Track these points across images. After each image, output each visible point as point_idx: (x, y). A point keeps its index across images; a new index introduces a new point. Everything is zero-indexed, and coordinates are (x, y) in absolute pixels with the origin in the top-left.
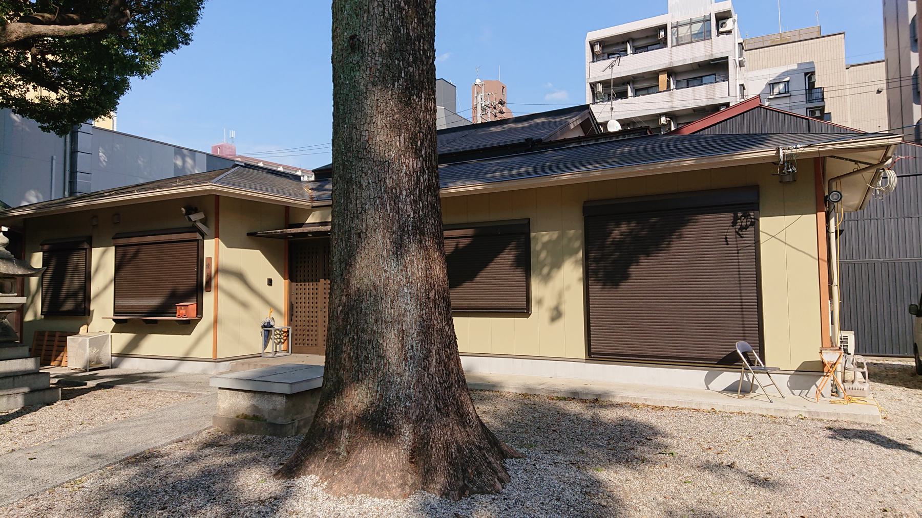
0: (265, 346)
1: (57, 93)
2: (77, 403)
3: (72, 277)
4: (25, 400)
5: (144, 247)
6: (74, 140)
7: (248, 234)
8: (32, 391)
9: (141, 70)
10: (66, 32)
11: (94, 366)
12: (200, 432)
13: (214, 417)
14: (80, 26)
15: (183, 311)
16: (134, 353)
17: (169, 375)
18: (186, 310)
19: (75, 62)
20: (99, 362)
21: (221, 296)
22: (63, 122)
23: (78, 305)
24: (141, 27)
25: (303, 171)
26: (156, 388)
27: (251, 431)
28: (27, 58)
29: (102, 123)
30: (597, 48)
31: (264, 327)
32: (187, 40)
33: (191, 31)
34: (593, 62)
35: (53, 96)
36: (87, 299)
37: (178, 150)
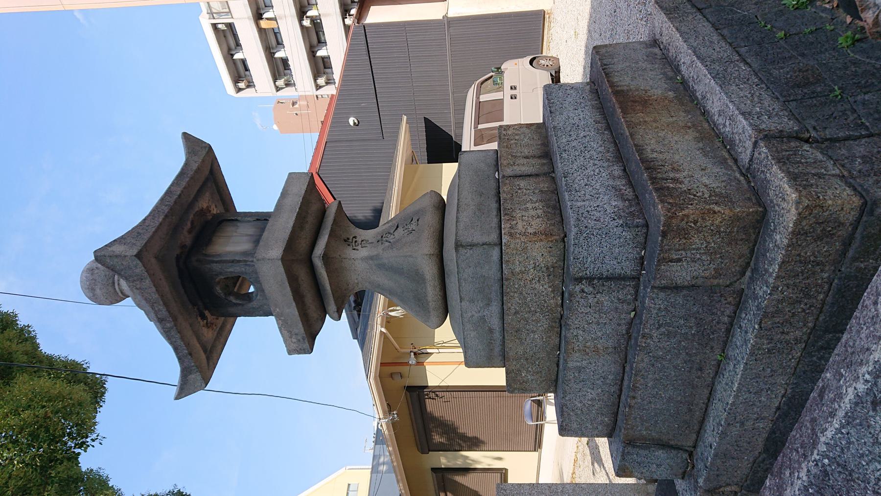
30: (242, 85)
34: (254, 86)
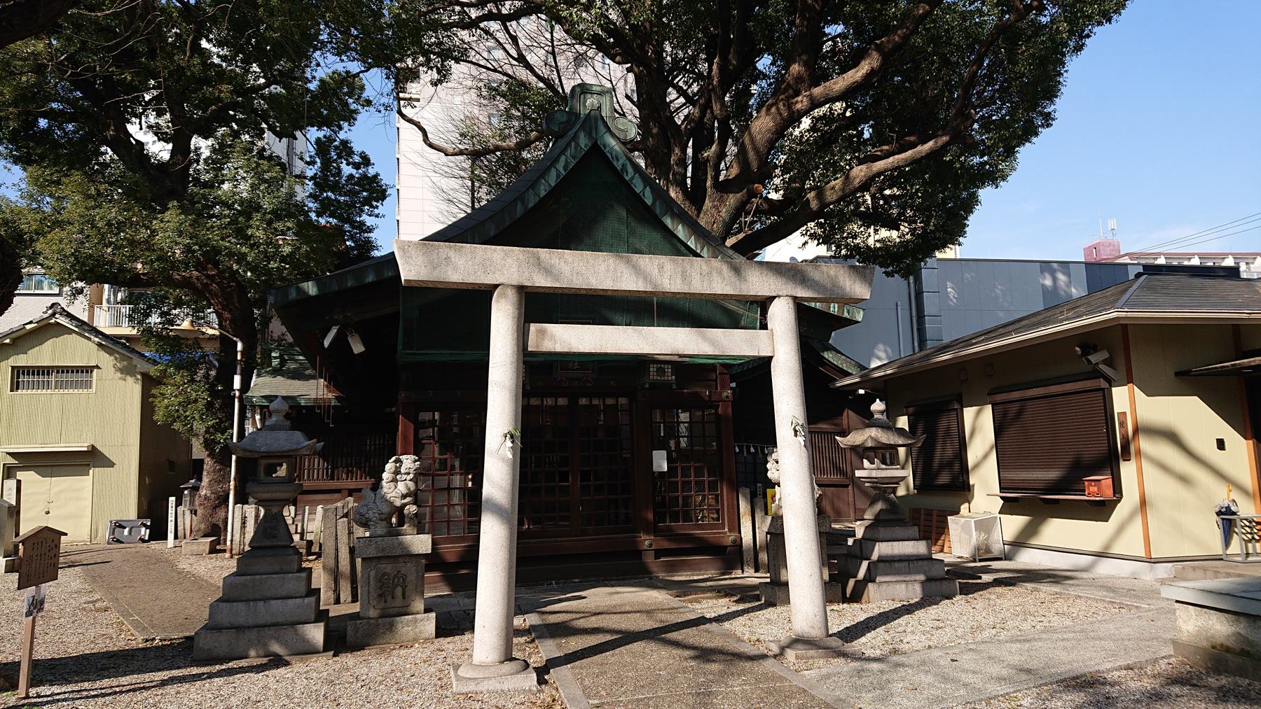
0: (1227, 543)
1: (898, 230)
2: (979, 599)
3: (944, 443)
4: (924, 589)
5: (1029, 403)
6: (918, 280)
7: (1177, 374)
8: (929, 580)
9: (993, 176)
10: (906, 160)
11: (983, 553)
12: (1156, 661)
13: (1175, 642)
14: (919, 148)
15: (1094, 489)
16: (1034, 542)
17: (1085, 575)
18: (1098, 486)
19: (917, 190)
20: (988, 550)
21: (1145, 465)
22: (904, 261)
23: (954, 478)
24: (986, 124)
25: (1236, 257)
26: (1073, 592)
27: (1241, 672)
28: (865, 201)
29: (949, 253)
31: (1219, 513)
32: (1048, 119)
33: (1053, 107)
35: (894, 234)
36: (965, 470)
37: (1046, 266)
